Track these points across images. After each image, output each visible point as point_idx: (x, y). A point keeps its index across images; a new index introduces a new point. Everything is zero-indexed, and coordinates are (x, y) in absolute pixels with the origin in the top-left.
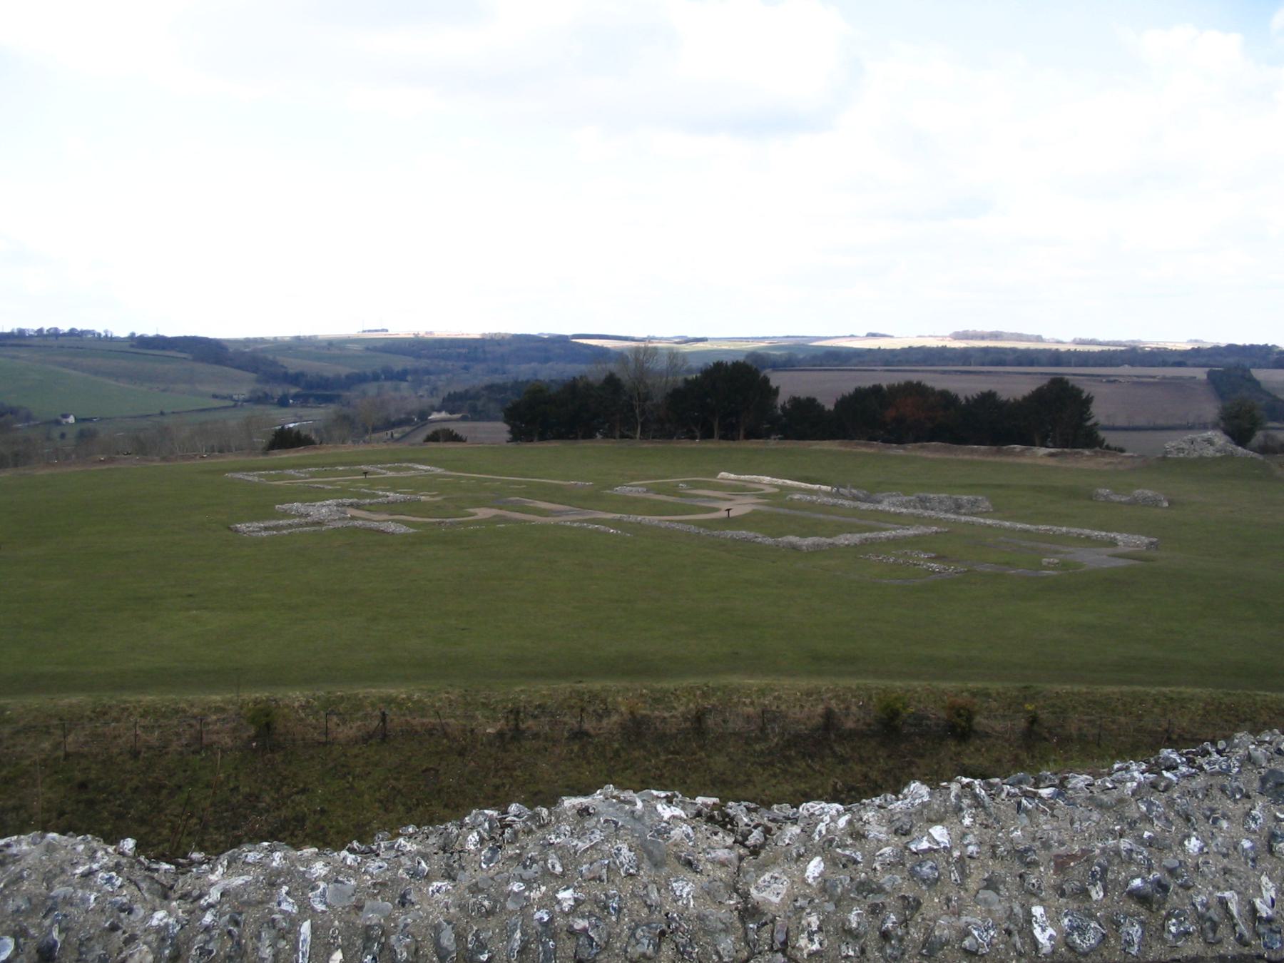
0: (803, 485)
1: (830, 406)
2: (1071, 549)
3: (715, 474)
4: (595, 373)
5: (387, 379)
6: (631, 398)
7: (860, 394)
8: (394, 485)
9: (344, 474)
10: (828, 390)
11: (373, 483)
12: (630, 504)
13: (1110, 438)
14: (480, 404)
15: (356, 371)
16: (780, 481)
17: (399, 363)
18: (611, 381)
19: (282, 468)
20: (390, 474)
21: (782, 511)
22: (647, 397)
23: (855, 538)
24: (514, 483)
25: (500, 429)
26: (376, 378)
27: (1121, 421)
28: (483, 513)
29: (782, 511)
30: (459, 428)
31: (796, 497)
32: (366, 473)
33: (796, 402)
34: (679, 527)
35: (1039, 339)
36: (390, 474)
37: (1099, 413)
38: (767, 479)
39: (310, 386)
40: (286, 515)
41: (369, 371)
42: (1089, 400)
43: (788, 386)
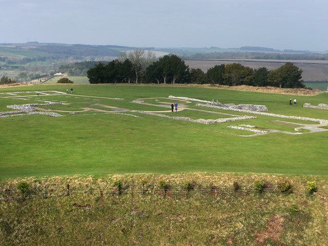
0: (200, 101)
1: (205, 72)
2: (304, 125)
3: (168, 97)
4: (122, 60)
5: (38, 60)
6: (134, 68)
7: (217, 68)
8: (49, 99)
9: (29, 94)
10: (205, 67)
11: (42, 98)
12: (138, 107)
13: (307, 85)
14: (73, 70)
15: (167, 54)
16: (191, 99)
17: (42, 55)
18: (127, 61)
19: (26, 91)
20: (47, 95)
21: (194, 109)
22: (140, 68)
23: (225, 120)
24: (85, 97)
25: (85, 79)
26: (34, 60)
27: (310, 80)
28: (87, 109)
29: (194, 109)
30: (71, 78)
31: (199, 105)
32: (38, 94)
33: (194, 71)
34: (160, 115)
35: (272, 50)
36: (47, 95)
37: (304, 77)
38: (186, 98)
39: (10, 62)
40: (10, 109)
41: (294, 50)
42: (301, 71)
43: (192, 65)
